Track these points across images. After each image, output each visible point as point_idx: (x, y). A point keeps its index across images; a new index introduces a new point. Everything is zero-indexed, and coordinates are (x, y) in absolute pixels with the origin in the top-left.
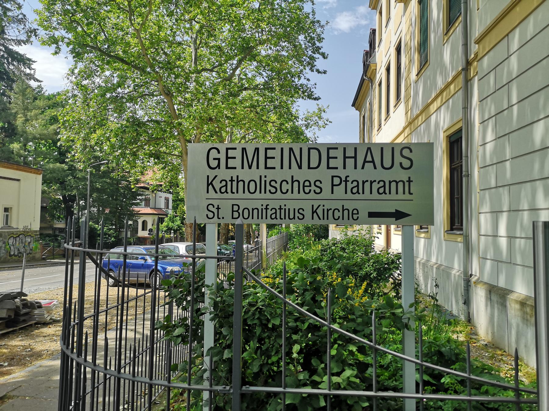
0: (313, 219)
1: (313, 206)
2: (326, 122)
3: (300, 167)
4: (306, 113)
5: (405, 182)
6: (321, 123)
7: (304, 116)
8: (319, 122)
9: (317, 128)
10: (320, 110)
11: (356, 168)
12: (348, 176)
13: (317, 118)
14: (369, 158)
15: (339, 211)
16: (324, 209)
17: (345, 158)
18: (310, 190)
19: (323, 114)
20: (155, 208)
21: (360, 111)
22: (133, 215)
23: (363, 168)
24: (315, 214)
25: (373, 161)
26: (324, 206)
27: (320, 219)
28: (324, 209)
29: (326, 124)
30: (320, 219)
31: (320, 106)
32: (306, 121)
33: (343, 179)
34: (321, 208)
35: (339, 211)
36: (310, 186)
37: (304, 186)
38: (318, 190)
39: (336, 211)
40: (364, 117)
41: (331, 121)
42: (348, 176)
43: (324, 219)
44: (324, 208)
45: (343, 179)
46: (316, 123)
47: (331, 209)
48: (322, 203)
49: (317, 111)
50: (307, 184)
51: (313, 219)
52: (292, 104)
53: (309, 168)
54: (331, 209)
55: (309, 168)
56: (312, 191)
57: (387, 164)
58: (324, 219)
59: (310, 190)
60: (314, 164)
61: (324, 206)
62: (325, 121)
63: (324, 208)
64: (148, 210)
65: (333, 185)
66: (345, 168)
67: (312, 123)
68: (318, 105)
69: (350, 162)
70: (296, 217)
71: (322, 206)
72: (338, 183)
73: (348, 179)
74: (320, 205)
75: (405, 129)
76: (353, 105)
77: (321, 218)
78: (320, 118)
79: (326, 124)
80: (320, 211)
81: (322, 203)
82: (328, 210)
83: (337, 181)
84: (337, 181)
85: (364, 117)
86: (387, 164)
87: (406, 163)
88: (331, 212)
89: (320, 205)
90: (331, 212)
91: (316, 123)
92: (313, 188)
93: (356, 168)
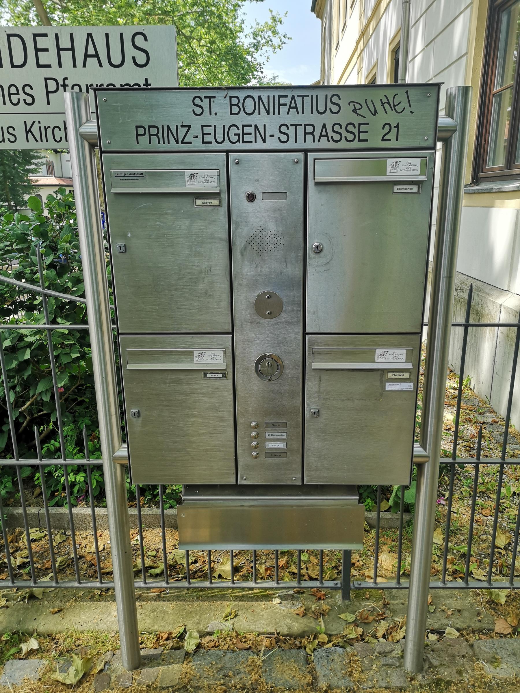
0: (28, 141)
1: (25, 122)
2: (283, 39)
3: (268, 113)
4: (254, 25)
5: (392, 127)
6: (276, 41)
7: (252, 30)
8: (273, 39)
9: (271, 49)
10: (274, 19)
11: (75, 66)
12: (66, 78)
13: (270, 33)
14: (91, 51)
15: (60, 130)
16: (40, 127)
17: (59, 50)
18: (19, 100)
19: (279, 27)
20: (62, 177)
21: (322, 19)
22: (30, 187)
23: (84, 66)
24: (30, 134)
25: (97, 56)
26: (39, 122)
27: (37, 141)
28: (40, 127)
29: (284, 43)
30: (37, 141)
31: (274, 13)
32: (254, 39)
33: (61, 83)
34: (36, 125)
35: (60, 130)
36: (18, 93)
37: (10, 94)
38: (29, 100)
39: (56, 129)
40: (325, 28)
41: (290, 37)
42: (66, 78)
43: (42, 141)
44: (40, 125)
45: (61, 83)
46: (268, 42)
47: (49, 127)
48: (36, 118)
49: (270, 22)
50: (13, 90)
51: (28, 141)
52: (236, 10)
53: (13, 66)
54: (49, 127)
55: (13, 66)
56: (22, 102)
57: (116, 59)
58: (42, 141)
59: (19, 100)
60: (18, 60)
61: (39, 122)
62: (282, 37)
63: (40, 125)
64: (52, 180)
65: (48, 92)
66: (60, 66)
67: (264, 41)
68: (271, 11)
69: (66, 56)
70: (6, 140)
71: (37, 123)
72: (54, 89)
73: (67, 82)
74: (34, 122)
75: (358, 43)
76: (313, 10)
77: (39, 140)
78: (275, 33)
79: (284, 43)
80: (35, 130)
81: (36, 118)
82: (46, 129)
83: (52, 86)
84: (52, 86)
85: (325, 28)
86: (116, 59)
87: (141, 58)
88: (50, 131)
89: (34, 122)
90: (50, 131)
91: (268, 42)
92: (22, 96)
93: (75, 66)
